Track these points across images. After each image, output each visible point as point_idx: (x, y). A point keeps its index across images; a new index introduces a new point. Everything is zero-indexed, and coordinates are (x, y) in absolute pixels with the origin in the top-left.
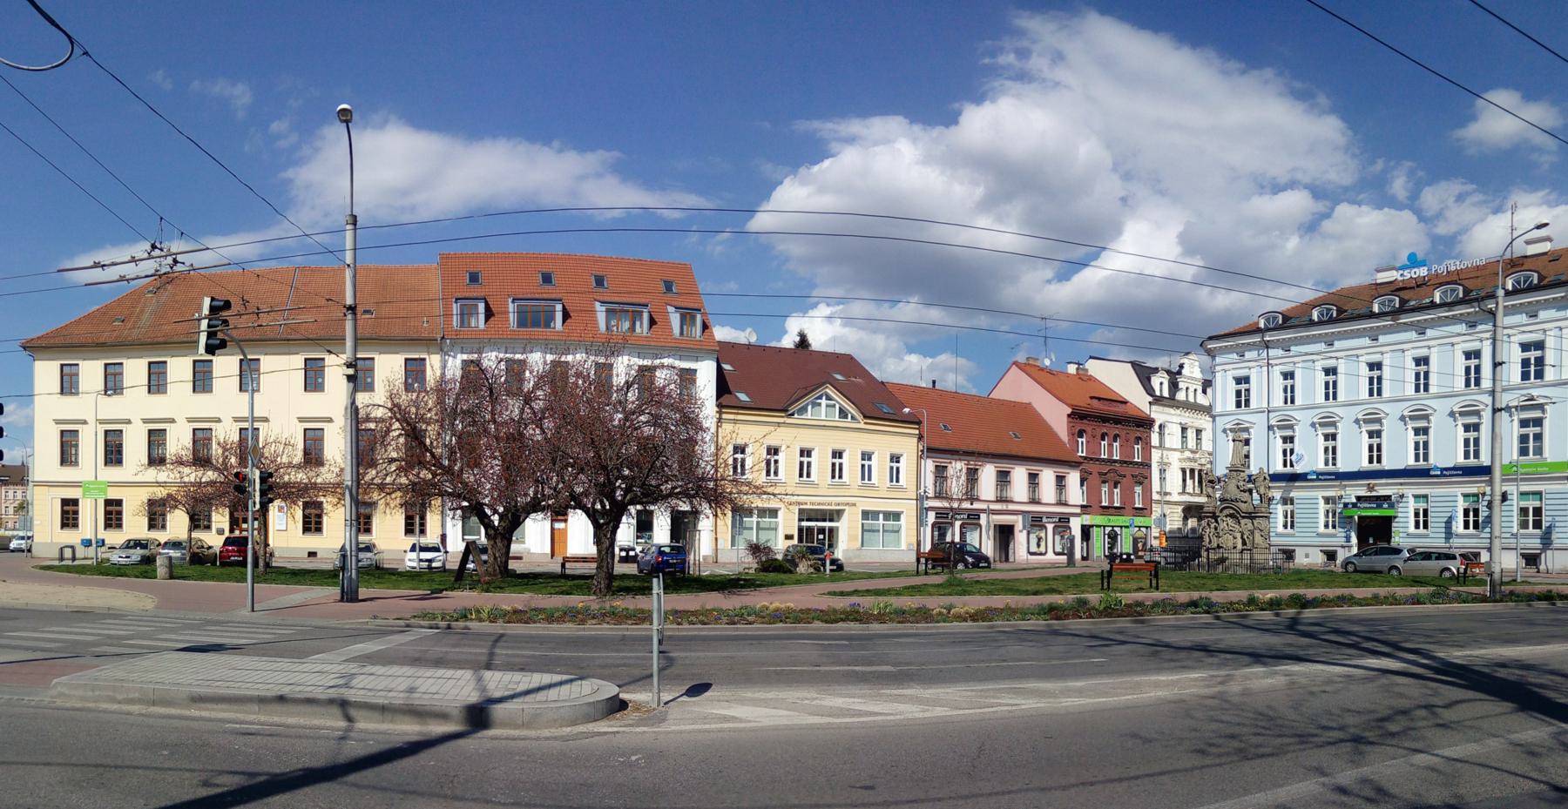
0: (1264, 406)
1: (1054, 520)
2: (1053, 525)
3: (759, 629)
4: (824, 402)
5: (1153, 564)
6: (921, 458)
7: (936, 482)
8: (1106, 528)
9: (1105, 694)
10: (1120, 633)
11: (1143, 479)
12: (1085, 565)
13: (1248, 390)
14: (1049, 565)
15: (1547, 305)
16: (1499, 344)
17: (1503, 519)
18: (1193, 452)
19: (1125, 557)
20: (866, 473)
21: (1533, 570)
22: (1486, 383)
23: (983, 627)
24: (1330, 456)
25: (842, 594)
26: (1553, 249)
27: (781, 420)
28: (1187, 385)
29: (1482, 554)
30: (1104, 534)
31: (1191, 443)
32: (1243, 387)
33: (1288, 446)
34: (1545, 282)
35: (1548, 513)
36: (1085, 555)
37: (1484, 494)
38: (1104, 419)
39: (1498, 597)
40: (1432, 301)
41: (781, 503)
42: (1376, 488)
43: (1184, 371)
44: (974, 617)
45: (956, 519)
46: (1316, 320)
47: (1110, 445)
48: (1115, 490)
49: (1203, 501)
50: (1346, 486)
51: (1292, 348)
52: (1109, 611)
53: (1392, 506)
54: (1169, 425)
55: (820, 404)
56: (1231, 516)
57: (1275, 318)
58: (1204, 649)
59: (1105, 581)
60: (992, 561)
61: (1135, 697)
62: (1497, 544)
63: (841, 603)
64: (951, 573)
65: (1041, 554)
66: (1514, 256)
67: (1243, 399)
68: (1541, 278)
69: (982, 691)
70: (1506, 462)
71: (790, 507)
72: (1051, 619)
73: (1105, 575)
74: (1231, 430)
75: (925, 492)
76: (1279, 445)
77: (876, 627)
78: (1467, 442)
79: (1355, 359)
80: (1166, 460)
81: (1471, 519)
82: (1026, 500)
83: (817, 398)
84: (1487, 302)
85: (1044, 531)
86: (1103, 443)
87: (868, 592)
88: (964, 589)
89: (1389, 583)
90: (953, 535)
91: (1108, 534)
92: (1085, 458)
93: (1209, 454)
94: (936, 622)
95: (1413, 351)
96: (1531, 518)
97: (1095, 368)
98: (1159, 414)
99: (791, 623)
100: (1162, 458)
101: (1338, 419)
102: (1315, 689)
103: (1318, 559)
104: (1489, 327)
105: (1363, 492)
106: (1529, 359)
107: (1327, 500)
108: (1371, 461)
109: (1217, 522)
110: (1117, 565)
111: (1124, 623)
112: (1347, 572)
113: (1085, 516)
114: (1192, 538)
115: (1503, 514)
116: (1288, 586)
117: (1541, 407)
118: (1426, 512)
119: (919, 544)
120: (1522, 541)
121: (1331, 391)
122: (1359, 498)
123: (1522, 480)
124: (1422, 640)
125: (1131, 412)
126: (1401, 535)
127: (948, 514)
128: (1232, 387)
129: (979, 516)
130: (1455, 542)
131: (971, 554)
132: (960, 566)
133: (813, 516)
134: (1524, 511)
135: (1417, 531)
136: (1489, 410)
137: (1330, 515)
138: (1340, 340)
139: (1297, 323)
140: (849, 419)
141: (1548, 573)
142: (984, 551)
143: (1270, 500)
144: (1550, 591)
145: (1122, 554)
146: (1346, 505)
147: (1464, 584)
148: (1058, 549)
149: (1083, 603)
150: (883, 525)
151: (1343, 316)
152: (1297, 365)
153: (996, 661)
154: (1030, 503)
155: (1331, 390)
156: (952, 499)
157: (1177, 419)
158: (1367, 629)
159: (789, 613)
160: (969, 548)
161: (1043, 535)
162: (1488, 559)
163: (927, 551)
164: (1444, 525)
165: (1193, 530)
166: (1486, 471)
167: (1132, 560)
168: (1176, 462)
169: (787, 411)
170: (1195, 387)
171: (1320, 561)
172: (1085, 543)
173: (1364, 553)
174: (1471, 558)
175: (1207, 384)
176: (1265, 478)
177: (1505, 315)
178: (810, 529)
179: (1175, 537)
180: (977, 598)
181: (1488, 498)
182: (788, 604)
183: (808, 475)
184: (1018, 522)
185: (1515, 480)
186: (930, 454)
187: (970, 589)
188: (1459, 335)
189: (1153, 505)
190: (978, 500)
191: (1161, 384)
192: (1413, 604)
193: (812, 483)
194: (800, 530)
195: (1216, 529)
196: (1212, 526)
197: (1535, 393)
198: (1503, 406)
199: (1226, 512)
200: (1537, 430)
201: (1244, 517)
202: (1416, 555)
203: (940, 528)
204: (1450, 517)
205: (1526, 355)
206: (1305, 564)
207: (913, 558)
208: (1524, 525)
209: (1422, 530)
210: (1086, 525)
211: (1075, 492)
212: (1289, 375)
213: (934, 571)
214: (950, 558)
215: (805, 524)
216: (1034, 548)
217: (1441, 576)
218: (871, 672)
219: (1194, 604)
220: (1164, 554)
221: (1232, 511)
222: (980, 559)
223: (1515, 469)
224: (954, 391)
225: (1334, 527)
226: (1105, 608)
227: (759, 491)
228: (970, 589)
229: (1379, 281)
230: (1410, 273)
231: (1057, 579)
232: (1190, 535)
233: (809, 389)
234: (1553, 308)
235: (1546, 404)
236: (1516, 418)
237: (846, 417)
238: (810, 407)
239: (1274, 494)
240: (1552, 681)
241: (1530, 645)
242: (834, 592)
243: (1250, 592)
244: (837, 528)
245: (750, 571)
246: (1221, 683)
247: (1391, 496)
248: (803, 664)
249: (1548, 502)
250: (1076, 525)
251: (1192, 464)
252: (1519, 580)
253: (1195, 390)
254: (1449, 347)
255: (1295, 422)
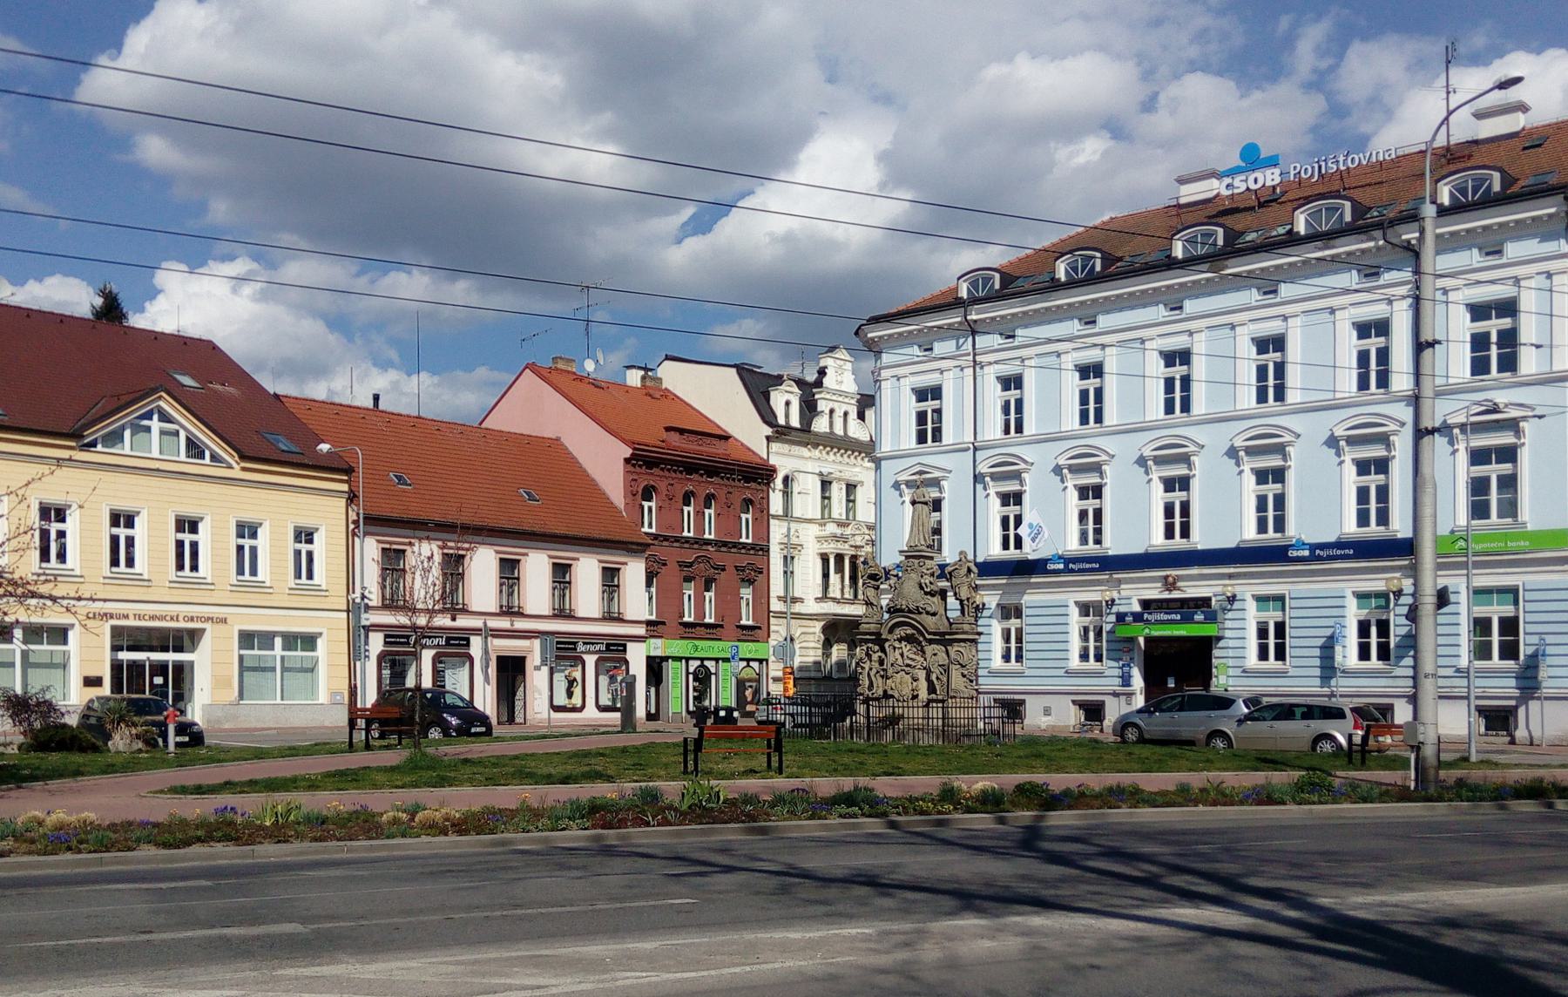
0: (966, 440)
1: (598, 648)
2: (596, 657)
3: (21, 866)
4: (155, 424)
5: (773, 727)
6: (354, 534)
7: (384, 580)
8: (691, 662)
9: (697, 964)
10: (724, 851)
11: (755, 574)
12: (653, 729)
13: (938, 412)
14: (589, 730)
15: (1521, 231)
16: (1426, 306)
17: (1441, 640)
18: (840, 524)
19: (722, 713)
20: (246, 561)
21: (1501, 740)
22: (1401, 381)
23: (484, 844)
24: (1091, 526)
25: (199, 790)
26: (1529, 126)
27: (65, 454)
28: (831, 405)
29: (1396, 708)
30: (688, 673)
31: (838, 508)
32: (930, 405)
33: (1012, 510)
34: (1515, 189)
35: (1530, 628)
36: (653, 711)
37: (1399, 593)
38: (690, 467)
39: (1432, 791)
40: (1290, 232)
41: (69, 614)
42: (1179, 584)
43: (826, 381)
44: (461, 826)
45: (424, 647)
46: (1063, 279)
47: (700, 514)
48: (707, 595)
49: (860, 613)
50: (1120, 581)
51: (1019, 332)
52: (702, 812)
53: (1211, 618)
54: (800, 477)
55: (148, 429)
56: (909, 639)
57: (987, 280)
58: (872, 881)
59: (691, 757)
60: (494, 721)
61: (748, 969)
62: (1428, 689)
63: (197, 809)
64: (417, 745)
65: (574, 709)
66: (1452, 143)
67: (929, 426)
68: (1508, 181)
69: (475, 962)
70: (1444, 530)
71: (90, 623)
72: (594, 827)
73: (691, 747)
74: (908, 484)
75: (363, 597)
76: (994, 510)
77: (269, 851)
78: (1363, 495)
79: (1138, 345)
80: (794, 540)
81: (1374, 640)
82: (547, 611)
83: (143, 417)
84: (1403, 227)
85: (580, 668)
86: (686, 509)
87: (252, 785)
88: (441, 775)
89: (1209, 764)
90: (419, 675)
91: (695, 674)
92: (655, 537)
93: (869, 528)
94: (388, 837)
95: (1252, 327)
96: (1495, 638)
97: (674, 377)
98: (783, 459)
99: (90, 852)
100: (788, 536)
101: (1104, 457)
102: (1080, 962)
103: (1067, 717)
104: (1406, 275)
105: (1154, 592)
106: (1487, 335)
107: (1085, 609)
108: (1169, 533)
109: (883, 650)
110: (710, 728)
111: (731, 833)
112: (1124, 741)
113: (652, 641)
114: (838, 679)
115: (1441, 630)
116: (1013, 768)
117: (1513, 425)
118: (1280, 628)
119: (353, 692)
120: (1479, 682)
121: (1092, 408)
122: (1146, 604)
123: (1477, 565)
124: (1283, 872)
125: (736, 455)
126: (1231, 672)
127: (408, 637)
128: (911, 406)
129: (468, 640)
130: (1341, 684)
131: (453, 710)
132: (435, 734)
133: (143, 640)
134: (1482, 625)
135: (1264, 665)
136: (1408, 432)
137: (1091, 635)
138: (1108, 312)
139: (1027, 287)
140: (207, 460)
141: (1531, 744)
142: (478, 704)
143: (979, 609)
144: (1541, 780)
145: (717, 709)
146: (1121, 618)
147: (1363, 765)
148: (605, 700)
149: (651, 798)
150: (283, 658)
151: (1116, 268)
152: (1027, 363)
153: (502, 907)
154: (555, 616)
155: (1092, 406)
156: (414, 610)
157: (811, 466)
158: (1176, 849)
159: (87, 833)
160: (449, 699)
161: (577, 674)
162: (1410, 718)
163: (369, 705)
164: (1317, 652)
165: (841, 665)
166: (1405, 548)
167: (735, 720)
168: (811, 542)
169: (83, 437)
170: (845, 408)
171: (1072, 722)
172: (653, 690)
173: (1158, 708)
174: (1375, 716)
175: (866, 402)
176: (969, 570)
177: (1438, 253)
178: (136, 667)
179: (810, 679)
180: (468, 790)
181: (1410, 600)
182: (85, 815)
183: (130, 562)
184: (533, 651)
185: (1465, 565)
186: (372, 529)
187: (452, 774)
188: (1347, 291)
189: (772, 621)
190: (465, 611)
191: (788, 403)
192: (1260, 803)
193: (202, 582)
194: (117, 667)
195: (881, 662)
196: (875, 657)
197: (1501, 397)
198: (1437, 425)
199: (900, 632)
200: (1506, 468)
201: (930, 642)
202: (1260, 709)
203: (395, 663)
204: (1331, 638)
205: (1482, 326)
206: (1043, 726)
207: (342, 718)
208: (1482, 651)
209: (1272, 663)
210: (655, 657)
211: (637, 600)
212: (1012, 382)
213: (384, 742)
214: (412, 718)
215: (125, 656)
216: (561, 699)
217: (1314, 749)
218: (258, 938)
219: (848, 799)
220: (790, 709)
221: (910, 631)
222: (471, 719)
223: (1462, 543)
224: (416, 414)
225: (1099, 658)
226: (690, 807)
227: (20, 591)
228: (452, 774)
229: (1183, 201)
230: (1246, 181)
231: (602, 755)
232: (835, 675)
233: (125, 399)
234: (1534, 236)
235: (1524, 418)
236: (1461, 446)
237: (201, 455)
238: (127, 433)
239: (986, 600)
240: (1552, 954)
241: (1500, 884)
242: (183, 787)
243: (945, 779)
244: (192, 664)
245: (9, 750)
246: (907, 945)
247: (1209, 599)
248: (117, 930)
249: (1530, 607)
250: (637, 657)
251: (839, 545)
252: (1473, 758)
253: (846, 414)
254: (1326, 316)
255: (1023, 466)
